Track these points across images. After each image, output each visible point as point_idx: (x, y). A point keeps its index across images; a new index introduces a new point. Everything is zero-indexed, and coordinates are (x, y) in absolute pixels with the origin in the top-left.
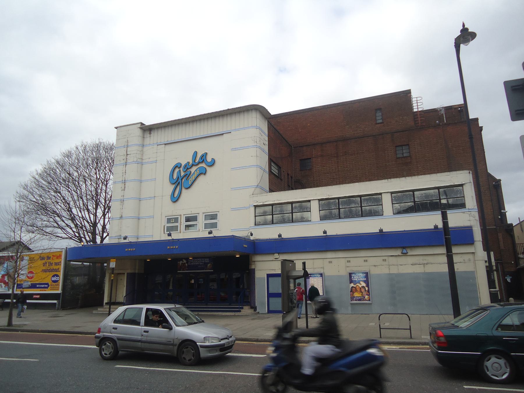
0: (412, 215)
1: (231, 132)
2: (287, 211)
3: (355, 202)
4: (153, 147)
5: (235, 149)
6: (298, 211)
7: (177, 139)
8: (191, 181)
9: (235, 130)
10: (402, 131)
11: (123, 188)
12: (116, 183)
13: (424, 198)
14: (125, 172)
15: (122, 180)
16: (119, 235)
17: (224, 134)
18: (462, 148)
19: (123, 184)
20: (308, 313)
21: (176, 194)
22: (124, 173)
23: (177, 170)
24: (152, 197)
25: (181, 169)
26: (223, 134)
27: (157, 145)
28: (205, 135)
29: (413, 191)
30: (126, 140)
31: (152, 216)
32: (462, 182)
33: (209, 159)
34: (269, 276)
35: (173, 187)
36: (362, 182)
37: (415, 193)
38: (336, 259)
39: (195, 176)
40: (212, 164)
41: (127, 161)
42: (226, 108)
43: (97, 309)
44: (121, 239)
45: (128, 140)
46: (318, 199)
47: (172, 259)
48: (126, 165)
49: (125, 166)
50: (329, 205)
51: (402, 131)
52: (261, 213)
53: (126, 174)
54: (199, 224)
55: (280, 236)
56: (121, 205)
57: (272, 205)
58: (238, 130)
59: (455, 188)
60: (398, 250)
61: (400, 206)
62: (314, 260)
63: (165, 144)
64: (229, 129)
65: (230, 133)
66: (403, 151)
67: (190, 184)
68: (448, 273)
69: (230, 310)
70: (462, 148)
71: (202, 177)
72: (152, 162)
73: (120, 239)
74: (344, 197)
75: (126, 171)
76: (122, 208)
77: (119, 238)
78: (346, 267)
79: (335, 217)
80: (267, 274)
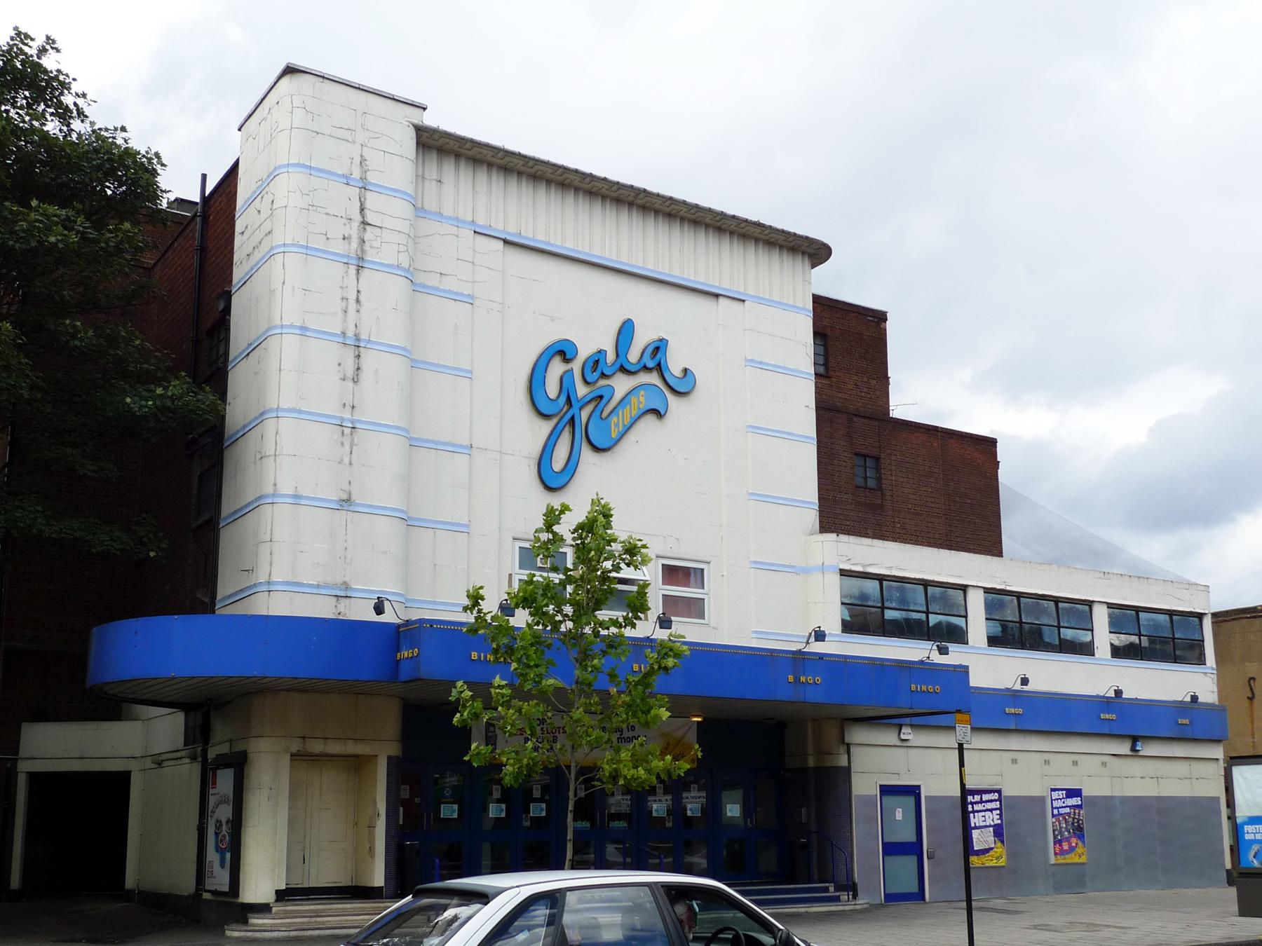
0: (1041, 657)
1: (744, 301)
2: (915, 604)
3: (1044, 611)
4: (454, 230)
5: (761, 363)
6: (940, 610)
7: (556, 242)
8: (617, 425)
9: (759, 300)
10: (868, 418)
11: (350, 370)
12: (308, 334)
13: (1152, 629)
14: (358, 301)
15: (344, 334)
16: (339, 580)
17: (721, 300)
18: (969, 501)
19: (350, 354)
20: (973, 898)
21: (558, 464)
22: (352, 306)
23: (557, 369)
24: (462, 447)
25: (576, 366)
26: (717, 296)
27: (475, 232)
28: (673, 276)
29: (1138, 610)
30: (355, 152)
31: (463, 525)
32: (1204, 609)
33: (675, 365)
34: (886, 790)
35: (545, 428)
36: (920, 545)
37: (1141, 615)
38: (1039, 753)
39: (634, 413)
40: (682, 387)
41: (363, 251)
42: (753, 217)
43: (245, 922)
44: (347, 601)
45: (366, 156)
46: (984, 588)
47: (704, 719)
48: (359, 268)
49: (353, 270)
50: (1001, 605)
51: (868, 418)
52: (855, 597)
53: (363, 310)
54: (709, 598)
55: (1118, 693)
56: (342, 444)
57: (881, 578)
58: (771, 303)
59: (1191, 618)
60: (1124, 742)
61: (1119, 640)
62: (984, 752)
63: (506, 242)
64: (737, 288)
65: (741, 303)
66: (866, 472)
67: (613, 436)
68: (960, 798)
69: (775, 899)
70: (969, 501)
71: (651, 419)
72: (456, 297)
73: (343, 601)
74: (1000, 590)
75: (362, 298)
76: (347, 460)
77: (342, 594)
78: (1042, 776)
79: (1013, 643)
80: (880, 786)
